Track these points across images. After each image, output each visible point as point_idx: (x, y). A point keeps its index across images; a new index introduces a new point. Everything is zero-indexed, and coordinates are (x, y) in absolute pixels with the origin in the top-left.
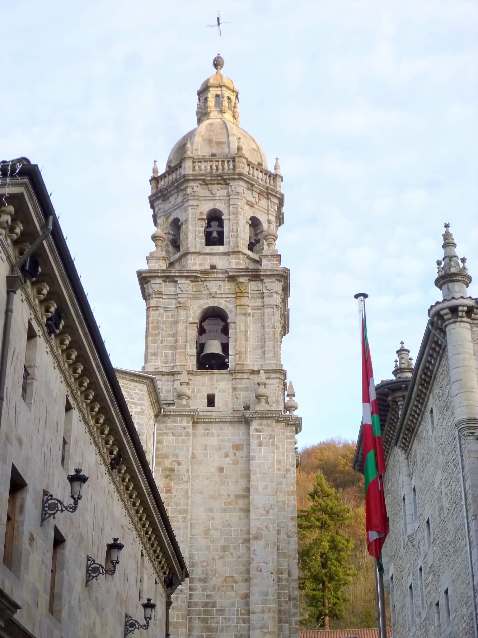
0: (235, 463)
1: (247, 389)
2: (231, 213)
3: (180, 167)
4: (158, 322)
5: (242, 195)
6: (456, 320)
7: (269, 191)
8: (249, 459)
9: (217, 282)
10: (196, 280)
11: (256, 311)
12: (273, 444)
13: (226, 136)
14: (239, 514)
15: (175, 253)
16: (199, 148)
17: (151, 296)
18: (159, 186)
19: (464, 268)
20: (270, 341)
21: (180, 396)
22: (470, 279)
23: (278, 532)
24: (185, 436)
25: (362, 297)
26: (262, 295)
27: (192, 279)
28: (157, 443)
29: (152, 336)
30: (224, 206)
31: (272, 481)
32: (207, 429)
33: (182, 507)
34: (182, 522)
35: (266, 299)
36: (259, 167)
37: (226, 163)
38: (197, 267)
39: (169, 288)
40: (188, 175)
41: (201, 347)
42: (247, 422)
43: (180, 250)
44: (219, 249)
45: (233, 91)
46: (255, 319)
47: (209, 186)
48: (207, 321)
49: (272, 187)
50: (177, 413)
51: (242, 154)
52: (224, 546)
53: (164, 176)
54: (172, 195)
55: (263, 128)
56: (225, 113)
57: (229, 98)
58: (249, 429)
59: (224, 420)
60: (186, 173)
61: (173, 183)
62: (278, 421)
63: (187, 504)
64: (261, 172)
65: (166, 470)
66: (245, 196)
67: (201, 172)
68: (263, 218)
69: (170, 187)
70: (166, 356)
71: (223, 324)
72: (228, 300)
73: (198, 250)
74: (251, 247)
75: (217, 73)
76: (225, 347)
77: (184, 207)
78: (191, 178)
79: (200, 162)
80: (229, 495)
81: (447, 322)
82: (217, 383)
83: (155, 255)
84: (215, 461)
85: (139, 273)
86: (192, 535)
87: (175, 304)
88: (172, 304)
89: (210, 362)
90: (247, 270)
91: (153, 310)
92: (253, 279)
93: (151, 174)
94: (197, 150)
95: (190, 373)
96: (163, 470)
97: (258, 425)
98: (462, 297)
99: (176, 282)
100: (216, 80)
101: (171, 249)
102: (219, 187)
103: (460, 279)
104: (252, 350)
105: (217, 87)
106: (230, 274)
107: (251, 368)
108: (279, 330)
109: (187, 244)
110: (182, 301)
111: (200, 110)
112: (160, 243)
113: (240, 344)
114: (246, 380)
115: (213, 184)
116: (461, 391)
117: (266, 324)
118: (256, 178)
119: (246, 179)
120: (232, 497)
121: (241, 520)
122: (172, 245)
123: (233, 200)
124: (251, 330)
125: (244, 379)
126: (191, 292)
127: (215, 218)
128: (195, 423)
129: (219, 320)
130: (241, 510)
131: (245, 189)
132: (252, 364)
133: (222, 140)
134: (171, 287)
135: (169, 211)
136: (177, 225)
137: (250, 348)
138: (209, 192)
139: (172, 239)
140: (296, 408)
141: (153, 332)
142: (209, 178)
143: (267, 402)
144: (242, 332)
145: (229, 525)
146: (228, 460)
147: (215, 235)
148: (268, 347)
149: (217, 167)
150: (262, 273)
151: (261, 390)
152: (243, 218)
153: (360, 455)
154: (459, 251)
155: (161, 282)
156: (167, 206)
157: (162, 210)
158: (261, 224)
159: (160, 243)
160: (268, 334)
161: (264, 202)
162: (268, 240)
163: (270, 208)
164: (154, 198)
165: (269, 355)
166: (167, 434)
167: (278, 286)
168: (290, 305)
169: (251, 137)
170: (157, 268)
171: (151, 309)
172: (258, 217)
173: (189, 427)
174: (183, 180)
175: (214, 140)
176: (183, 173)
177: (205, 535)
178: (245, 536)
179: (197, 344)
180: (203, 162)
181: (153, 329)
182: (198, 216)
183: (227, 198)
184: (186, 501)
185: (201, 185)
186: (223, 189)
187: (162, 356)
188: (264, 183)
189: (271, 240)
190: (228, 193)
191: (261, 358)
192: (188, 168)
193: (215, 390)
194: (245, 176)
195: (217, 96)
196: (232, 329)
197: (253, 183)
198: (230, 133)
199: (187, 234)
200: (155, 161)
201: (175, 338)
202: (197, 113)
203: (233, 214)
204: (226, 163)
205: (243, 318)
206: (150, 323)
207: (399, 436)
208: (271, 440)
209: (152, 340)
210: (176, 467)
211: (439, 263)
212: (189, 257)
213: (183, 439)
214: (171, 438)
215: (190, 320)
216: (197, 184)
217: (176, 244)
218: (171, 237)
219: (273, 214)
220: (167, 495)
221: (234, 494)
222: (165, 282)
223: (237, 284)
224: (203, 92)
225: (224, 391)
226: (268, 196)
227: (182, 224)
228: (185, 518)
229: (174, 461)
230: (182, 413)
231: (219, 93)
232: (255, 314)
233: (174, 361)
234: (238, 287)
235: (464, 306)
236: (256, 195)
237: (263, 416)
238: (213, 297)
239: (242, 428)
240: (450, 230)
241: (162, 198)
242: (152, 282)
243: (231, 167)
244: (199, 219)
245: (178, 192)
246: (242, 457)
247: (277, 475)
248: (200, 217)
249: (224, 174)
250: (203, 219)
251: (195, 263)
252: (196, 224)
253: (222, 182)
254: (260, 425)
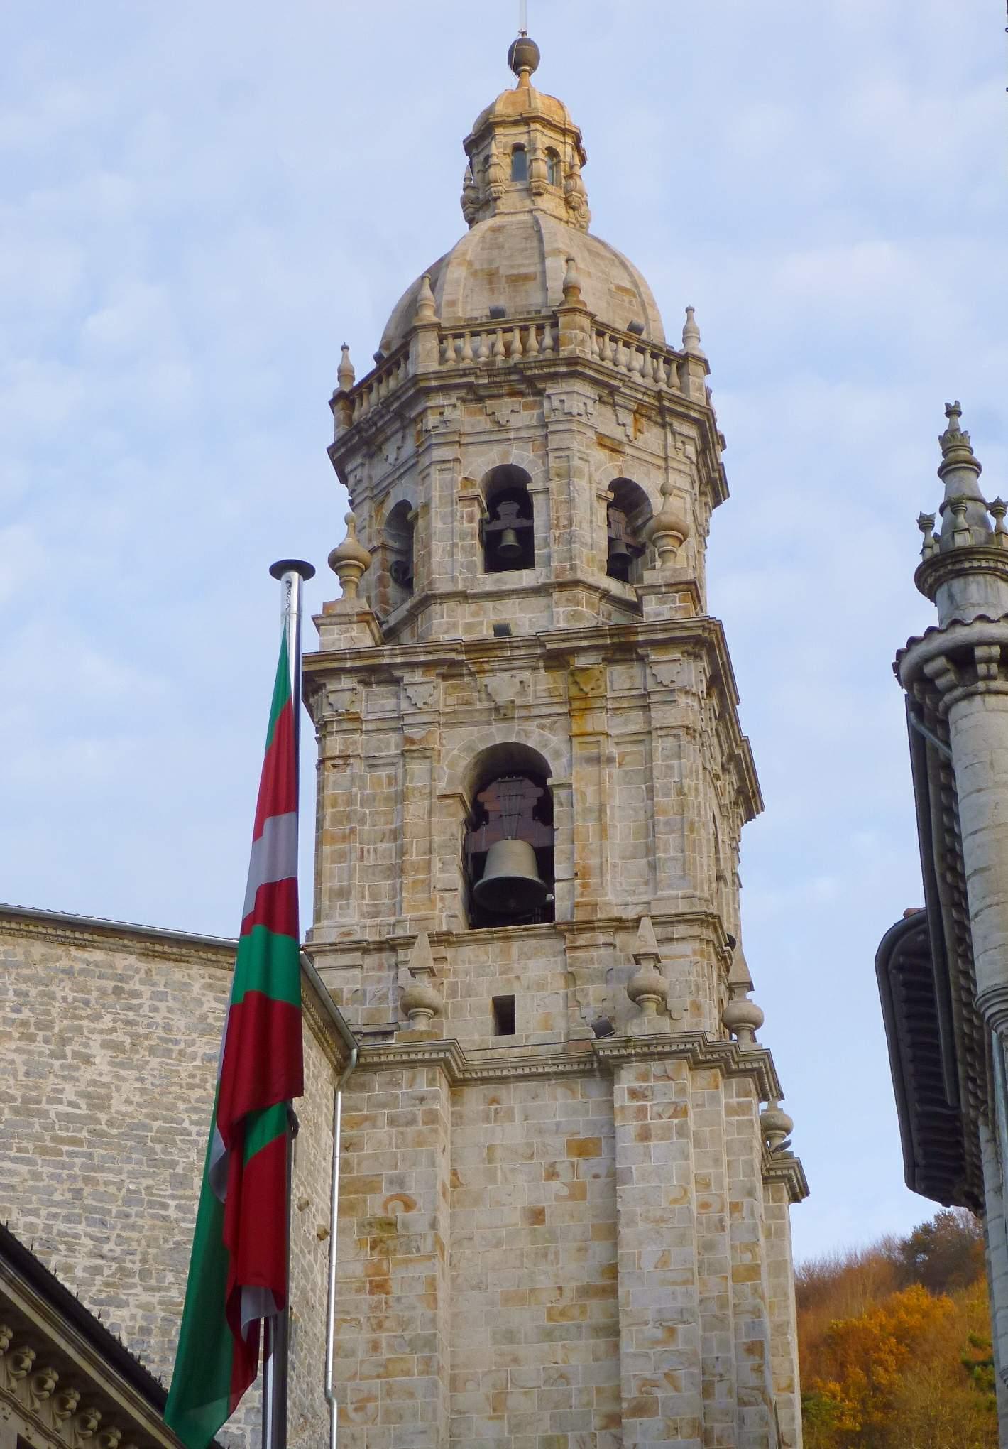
0: (578, 1192)
1: (606, 976)
2: (552, 472)
3: (406, 357)
4: (350, 801)
5: (584, 419)
6: (972, 688)
7: (666, 403)
8: (614, 1178)
9: (514, 673)
10: (455, 671)
11: (629, 748)
12: (682, 1131)
13: (537, 259)
14: (592, 1341)
15: (404, 601)
16: (466, 300)
17: (329, 727)
18: (356, 415)
20: (672, 832)
21: (410, 1007)
23: (707, 1391)
24: (425, 1123)
25: (295, 576)
26: (644, 702)
27: (444, 670)
28: (345, 1148)
29: (334, 840)
30: (531, 455)
31: (682, 1239)
32: (494, 1101)
33: (417, 1330)
34: (421, 1373)
35: (656, 713)
36: (634, 337)
37: (533, 332)
38: (461, 635)
39: (379, 702)
40: (426, 376)
41: (475, 863)
42: (605, 1071)
43: (412, 593)
44: (521, 577)
45: (565, 132)
46: (626, 772)
47: (489, 403)
48: (494, 785)
49: (675, 391)
50: (398, 1058)
51: (579, 302)
52: (551, 1438)
53: (367, 385)
54: (387, 439)
55: (658, 233)
56: (540, 194)
57: (552, 153)
58: (612, 1094)
59: (541, 1070)
60: (420, 371)
61: (387, 403)
62: (696, 1065)
63: (433, 1320)
64: (641, 350)
65: (370, 1224)
66: (592, 421)
67: (462, 365)
68: (648, 482)
69: (382, 417)
70: (374, 896)
71: (540, 792)
72: (547, 721)
73: (460, 587)
74: (619, 566)
75: (519, 86)
76: (544, 859)
77: (420, 467)
78: (434, 383)
79: (460, 336)
80: (560, 1288)
81: (947, 698)
82: (526, 966)
83: (338, 610)
84: (519, 1190)
86: (459, 1412)
87: (397, 746)
88: (388, 745)
89: (504, 906)
90: (597, 633)
91: (335, 767)
92: (618, 657)
93: (332, 385)
94: (453, 303)
95: (440, 939)
96: (361, 1225)
97: (637, 1079)
98: (982, 618)
99: (397, 681)
100: (513, 104)
101: (392, 590)
102: (516, 402)
103: (984, 564)
104: (619, 862)
105: (515, 123)
106: (549, 647)
107: (616, 912)
108: (706, 799)
109: (429, 573)
110: (416, 734)
111: (472, 194)
112: (352, 575)
113: (584, 847)
114: (602, 951)
115: (500, 396)
116: (988, 901)
117: (658, 784)
118: (624, 370)
119: (590, 373)
120: (569, 1293)
121: (596, 1359)
122: (396, 580)
123: (556, 437)
124: (617, 803)
125: (597, 946)
126: (441, 708)
127: (508, 492)
128: (456, 1085)
129: (528, 783)
130: (598, 1331)
131: (590, 403)
132: (619, 901)
133: (524, 270)
134: (384, 698)
135: (385, 484)
136: (404, 521)
137: (613, 856)
138: (488, 419)
139: (396, 563)
140: (758, 1024)
141: (336, 830)
142: (486, 381)
143: (664, 1010)
144: (590, 810)
145: (562, 1376)
146: (555, 1185)
147: (510, 539)
148: (666, 851)
149: (508, 347)
150: (641, 638)
151: (646, 975)
152: (587, 486)
153: (915, 1145)
155: (355, 685)
156: (380, 470)
157: (365, 484)
158: (647, 499)
159: (352, 575)
160: (665, 812)
161: (652, 437)
162: (660, 543)
163: (671, 452)
164: (343, 450)
165: (668, 873)
166: (371, 1120)
167: (693, 673)
168: (747, 726)
169: (616, 255)
170: (343, 646)
171: (329, 763)
172: (635, 479)
173: (435, 1097)
174: (411, 392)
175: (502, 272)
176: (411, 372)
177: (494, 1410)
178: (609, 1408)
179: (465, 856)
180: (468, 337)
181: (337, 820)
182: (459, 491)
183: (540, 433)
184: (429, 1313)
185: (464, 401)
186: (527, 407)
187: (363, 897)
188: (648, 382)
189: (670, 541)
190: (542, 417)
191: (647, 883)
192: (426, 357)
193: (516, 984)
194: (588, 364)
195: (518, 148)
196: (561, 805)
197: (615, 383)
198: (547, 248)
199: (427, 546)
200: (345, 348)
201: (399, 842)
202: (465, 203)
203: (558, 475)
204: (533, 332)
205: (591, 770)
206: (327, 803)
207: (955, 1074)
208: (675, 1121)
209: (333, 852)
210: (400, 1214)
211: (925, 523)
212: (436, 608)
213: (420, 1133)
214: (383, 1132)
215: (442, 787)
216: (454, 401)
217: (403, 574)
218: (392, 558)
219: (682, 467)
220: (375, 1298)
221: (574, 1284)
222: (366, 683)
223: (572, 674)
224: (477, 143)
225: (541, 986)
226: (663, 419)
227: (416, 517)
228: (428, 1362)
229: (392, 1198)
230: (413, 1057)
231: (523, 139)
232: (628, 758)
233: (396, 908)
234: (576, 683)
235: (990, 644)
236: (627, 418)
237: (652, 1051)
238: (506, 718)
239: (595, 1089)
240: (963, 423)
241: (364, 450)
242: (329, 687)
243: (548, 341)
244: (461, 499)
245: (404, 428)
246: (596, 1176)
247: (700, 1223)
248: (464, 493)
249: (527, 365)
250: (475, 498)
251: (451, 625)
252: (453, 513)
253: (523, 387)
254: (644, 1077)
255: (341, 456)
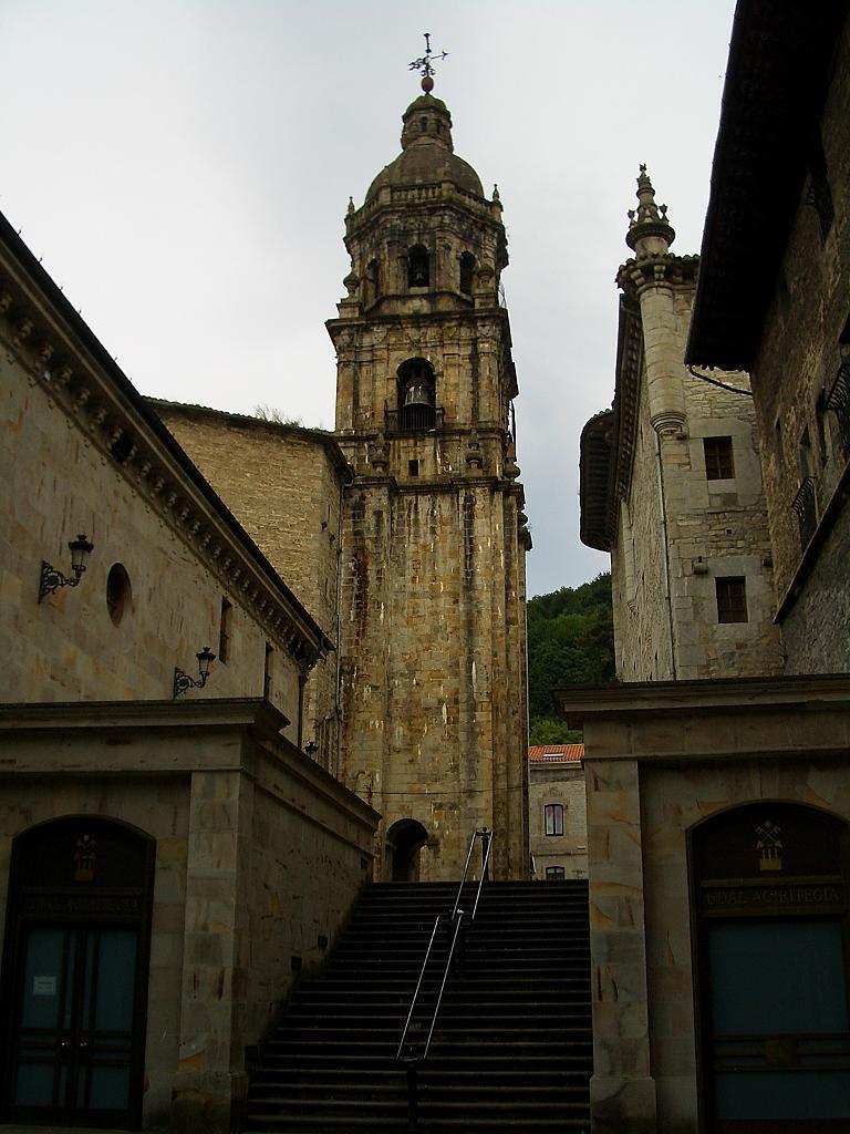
19: (665, 218)
22: (672, 233)
81: (640, 289)
85: (328, 323)
154: (658, 200)
167: (487, 330)
168: (516, 355)
211: (631, 214)
255: (348, 241)
